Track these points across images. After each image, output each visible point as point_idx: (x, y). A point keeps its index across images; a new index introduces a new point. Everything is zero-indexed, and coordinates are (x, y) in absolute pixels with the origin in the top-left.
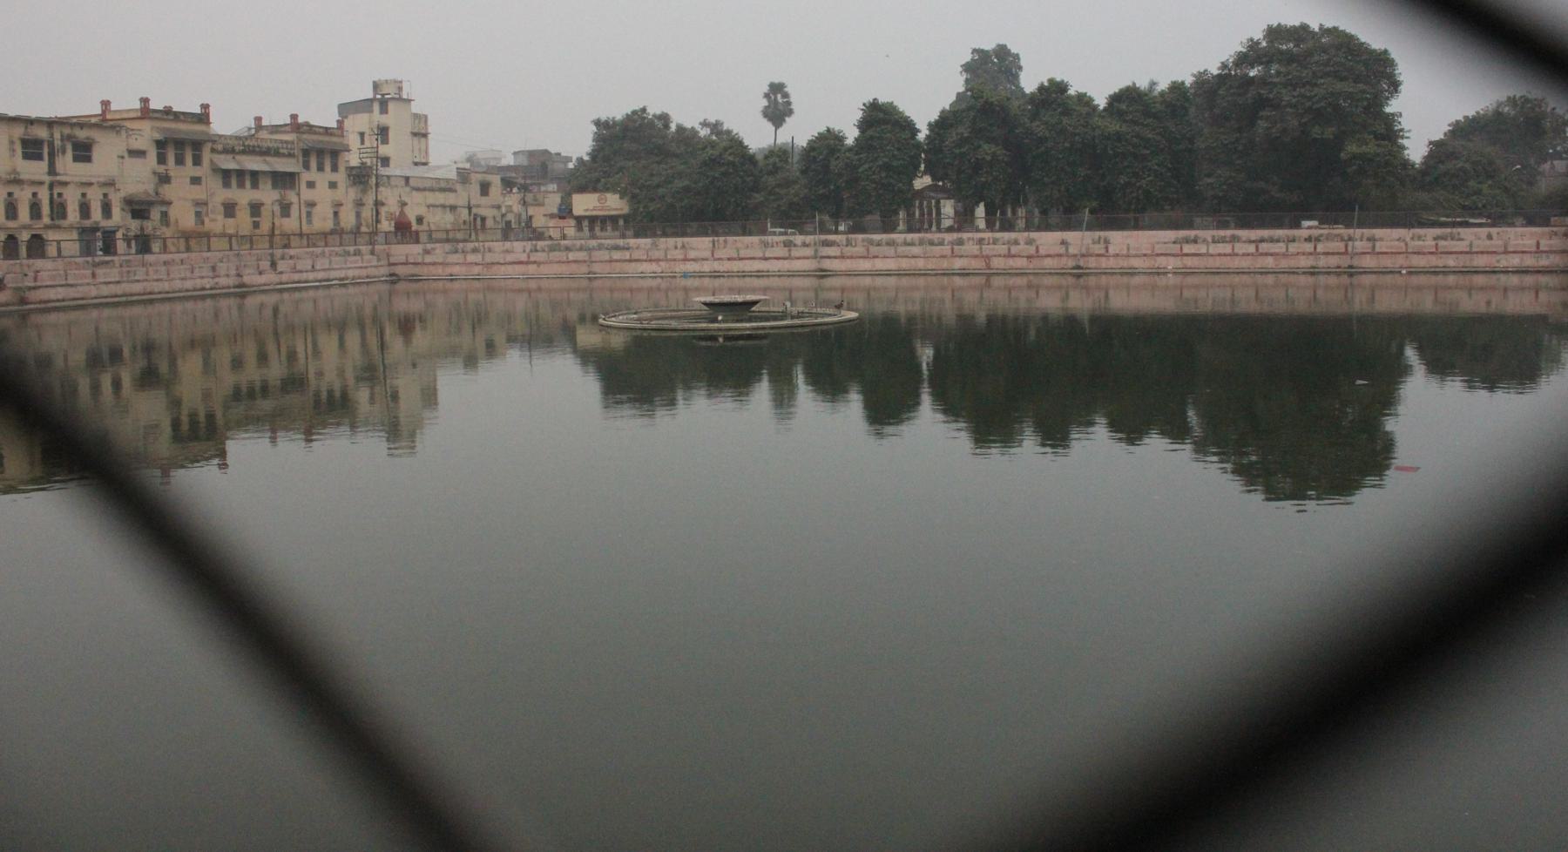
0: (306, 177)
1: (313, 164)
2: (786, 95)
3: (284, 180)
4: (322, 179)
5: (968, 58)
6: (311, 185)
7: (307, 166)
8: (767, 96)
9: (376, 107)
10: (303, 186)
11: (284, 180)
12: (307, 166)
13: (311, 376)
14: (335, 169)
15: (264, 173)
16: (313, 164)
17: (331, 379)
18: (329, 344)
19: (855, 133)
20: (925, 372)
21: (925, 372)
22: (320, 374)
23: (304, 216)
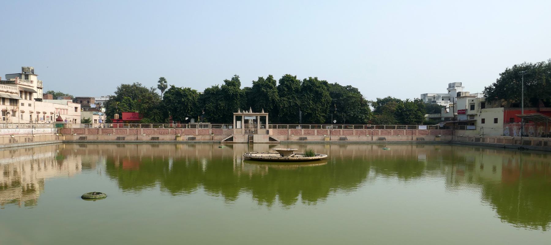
0: (21, 101)
1: (24, 96)
2: (165, 82)
3: (14, 101)
4: (26, 102)
5: (313, 78)
6: (23, 104)
7: (21, 97)
8: (159, 82)
9: (23, 77)
10: (20, 104)
11: (14, 101)
12: (21, 97)
13: (22, 180)
14: (30, 99)
15: (7, 99)
16: (24, 96)
17: (28, 181)
18: (28, 168)
19: (243, 88)
20: (301, 118)
21: (301, 118)
22: (24, 180)
23: (20, 117)
